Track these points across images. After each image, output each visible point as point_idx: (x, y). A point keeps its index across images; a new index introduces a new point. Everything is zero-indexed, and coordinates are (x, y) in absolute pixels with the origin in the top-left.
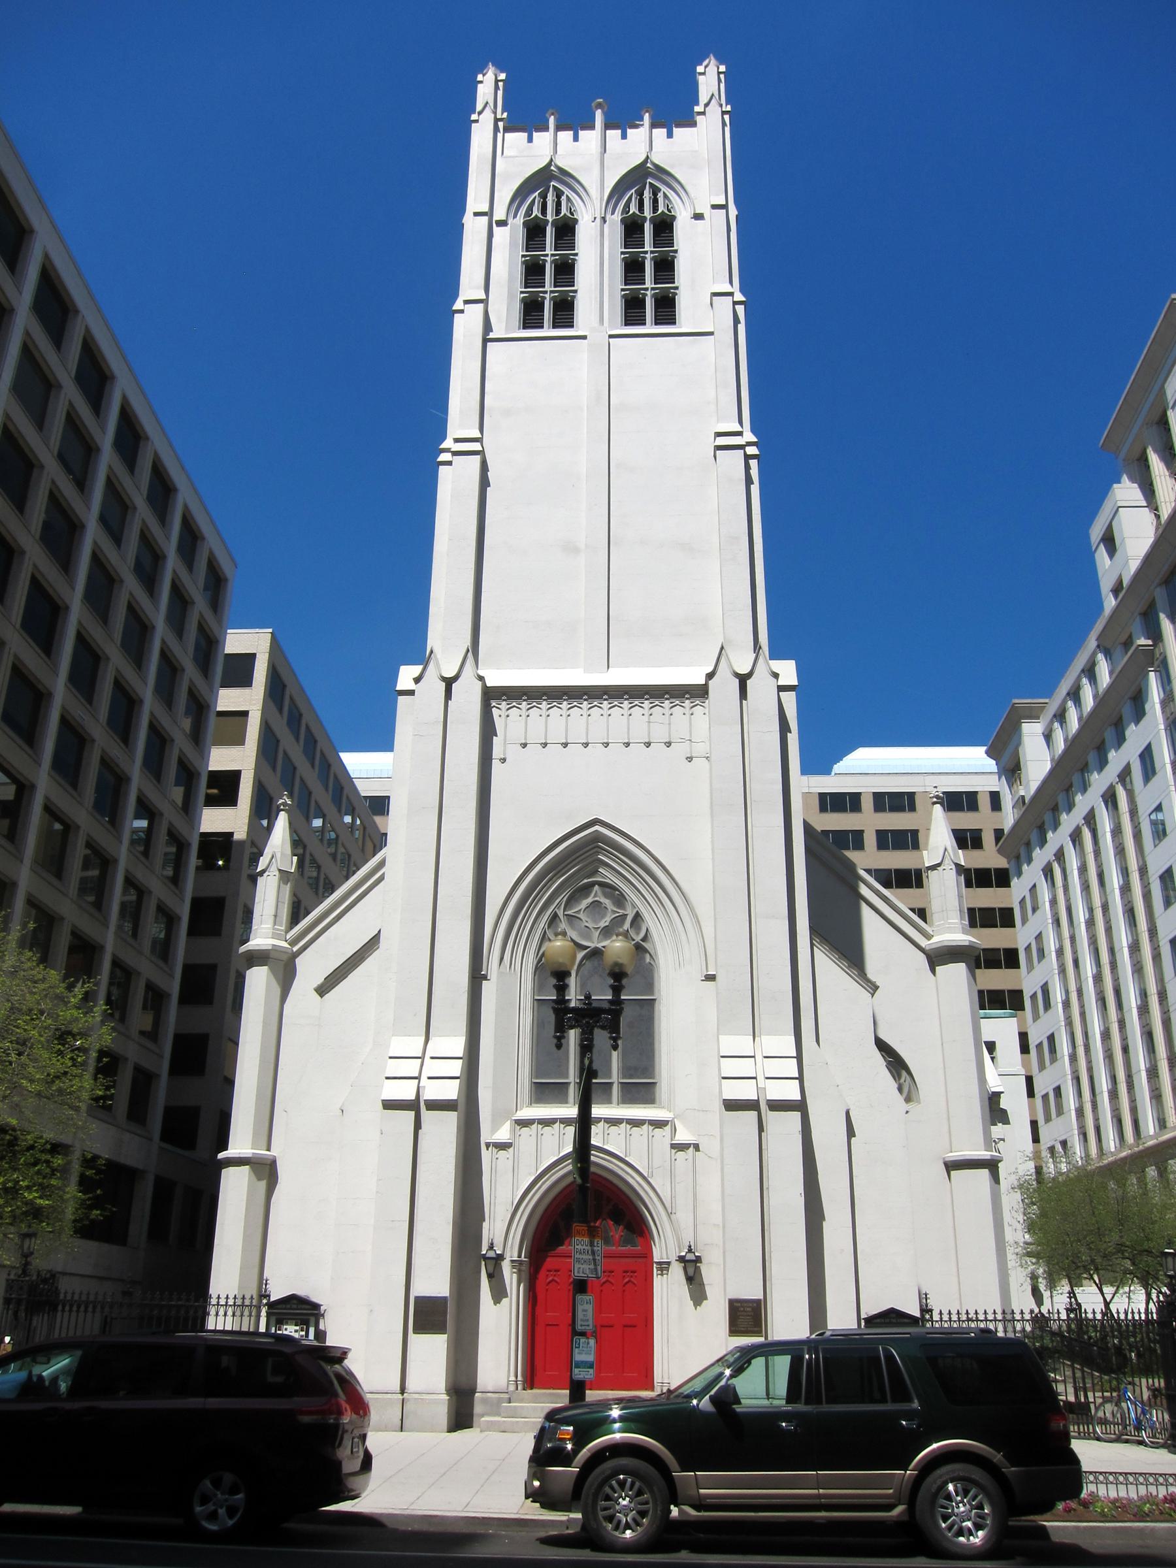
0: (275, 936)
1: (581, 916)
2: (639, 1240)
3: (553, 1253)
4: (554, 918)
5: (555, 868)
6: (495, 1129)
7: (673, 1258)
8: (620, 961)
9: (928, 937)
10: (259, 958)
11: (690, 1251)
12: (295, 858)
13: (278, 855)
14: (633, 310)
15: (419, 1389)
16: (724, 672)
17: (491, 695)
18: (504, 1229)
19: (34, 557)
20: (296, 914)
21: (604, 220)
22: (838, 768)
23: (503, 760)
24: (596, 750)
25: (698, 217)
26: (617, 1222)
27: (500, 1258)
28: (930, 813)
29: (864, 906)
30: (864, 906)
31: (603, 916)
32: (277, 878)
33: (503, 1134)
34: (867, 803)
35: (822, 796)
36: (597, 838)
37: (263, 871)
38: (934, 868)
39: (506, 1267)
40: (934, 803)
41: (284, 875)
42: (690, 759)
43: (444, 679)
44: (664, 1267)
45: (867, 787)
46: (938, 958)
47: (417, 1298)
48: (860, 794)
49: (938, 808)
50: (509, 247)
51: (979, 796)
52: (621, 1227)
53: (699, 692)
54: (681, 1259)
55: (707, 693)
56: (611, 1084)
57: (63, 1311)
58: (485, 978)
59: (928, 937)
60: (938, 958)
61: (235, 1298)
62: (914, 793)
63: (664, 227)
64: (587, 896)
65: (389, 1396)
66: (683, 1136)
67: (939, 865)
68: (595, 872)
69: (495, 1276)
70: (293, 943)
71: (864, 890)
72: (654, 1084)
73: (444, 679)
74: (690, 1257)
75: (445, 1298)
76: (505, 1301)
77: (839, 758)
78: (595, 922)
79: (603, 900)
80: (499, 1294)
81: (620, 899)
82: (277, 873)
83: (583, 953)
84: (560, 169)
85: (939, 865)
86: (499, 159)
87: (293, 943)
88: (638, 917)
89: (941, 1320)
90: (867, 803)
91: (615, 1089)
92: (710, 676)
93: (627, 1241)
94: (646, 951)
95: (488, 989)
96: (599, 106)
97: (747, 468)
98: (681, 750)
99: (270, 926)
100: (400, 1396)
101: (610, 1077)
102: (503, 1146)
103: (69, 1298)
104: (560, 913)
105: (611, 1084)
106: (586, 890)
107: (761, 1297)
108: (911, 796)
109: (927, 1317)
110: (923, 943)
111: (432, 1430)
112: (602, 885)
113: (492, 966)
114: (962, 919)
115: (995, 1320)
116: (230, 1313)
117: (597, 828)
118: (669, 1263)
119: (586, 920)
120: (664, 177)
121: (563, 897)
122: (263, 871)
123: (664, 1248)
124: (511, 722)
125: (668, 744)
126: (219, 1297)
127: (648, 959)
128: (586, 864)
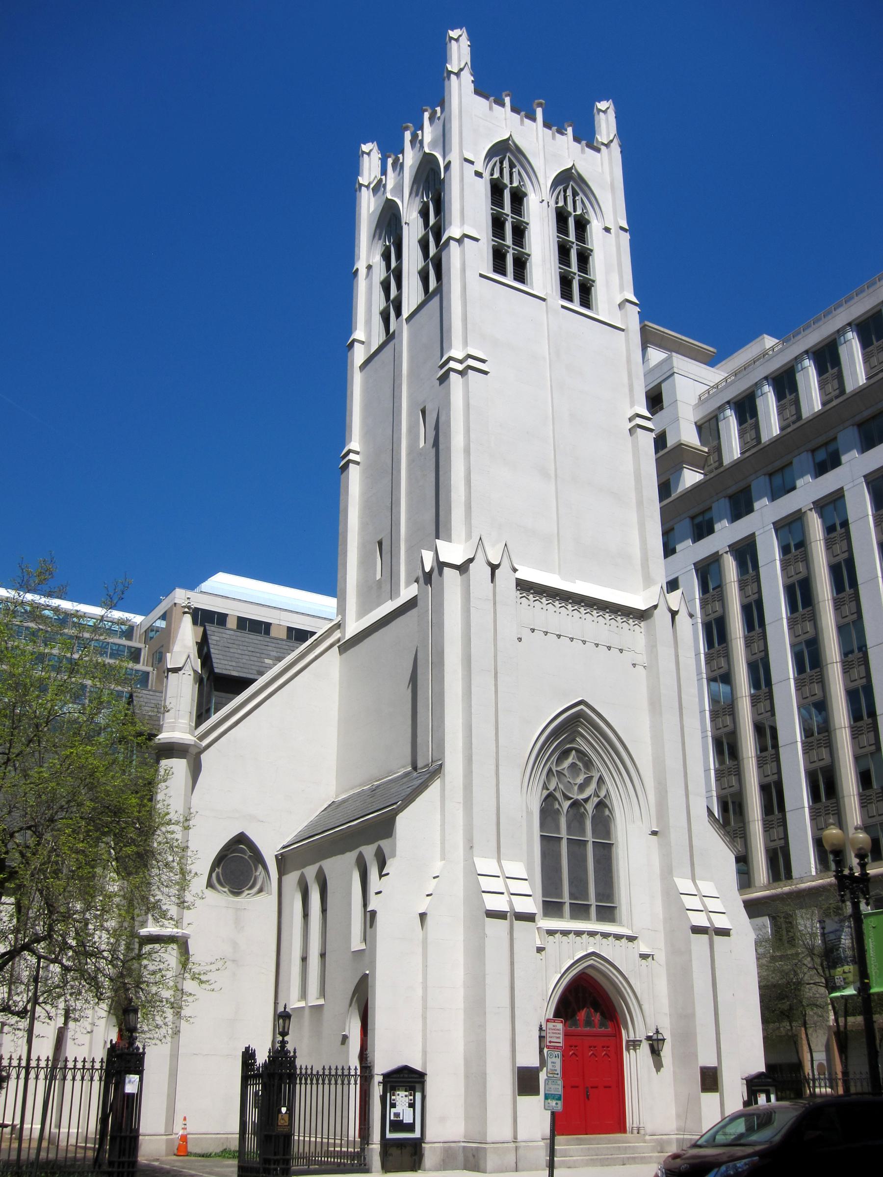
1: (566, 772)
2: (609, 1023)
4: (550, 770)
5: (555, 734)
7: (643, 1038)
10: (172, 750)
11: (657, 1032)
15: (493, 1140)
20: (202, 715)
22: (206, 586)
25: (607, 230)
28: (181, 620)
31: (578, 776)
38: (176, 670)
40: (185, 613)
42: (634, 665)
44: (634, 1044)
45: (234, 611)
49: (188, 619)
52: (598, 1014)
53: (642, 615)
54: (649, 1038)
56: (589, 906)
57: (301, 1084)
61: (84, 1061)
62: (270, 624)
65: (506, 1145)
66: (645, 950)
67: (180, 669)
68: (573, 740)
70: (202, 738)
72: (614, 908)
77: (205, 579)
79: (578, 763)
81: (588, 764)
82: (192, 673)
83: (569, 802)
85: (180, 669)
87: (202, 738)
88: (601, 780)
89: (10, 1066)
91: (593, 910)
93: (602, 1025)
94: (606, 806)
96: (540, 105)
100: (513, 1145)
101: (562, 898)
103: (309, 1072)
104: (554, 769)
105: (589, 906)
106: (565, 754)
108: (268, 625)
111: (537, 1169)
112: (578, 751)
114: (191, 720)
116: (78, 1077)
117: (582, 707)
118: (641, 1041)
120: (586, 189)
121: (555, 757)
123: (638, 1028)
125: (621, 651)
126: (75, 1061)
127: (607, 812)
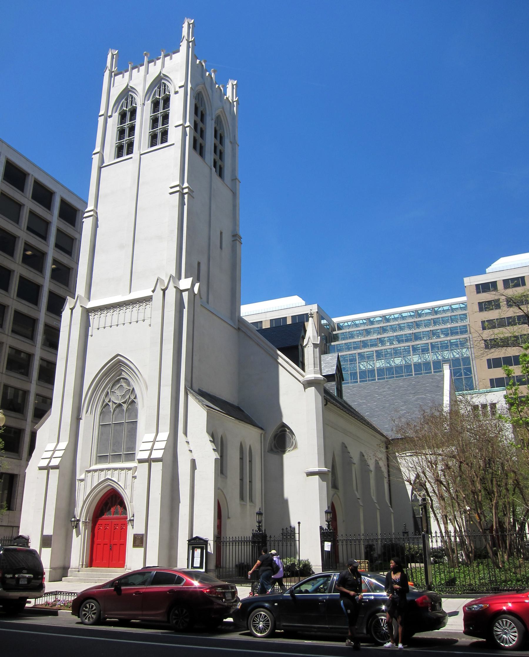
0: (315, 373)
3: (101, 518)
5: (106, 374)
6: (81, 475)
9: (303, 376)
12: (319, 337)
13: (311, 338)
17: (87, 312)
18: (82, 510)
21: (144, 104)
22: (488, 270)
23: (92, 336)
26: (121, 506)
27: (79, 520)
29: (280, 367)
30: (280, 366)
32: (312, 347)
33: (83, 477)
34: (500, 286)
35: (477, 286)
36: (120, 361)
37: (306, 345)
39: (81, 523)
41: (315, 346)
43: (162, 290)
45: (499, 278)
46: (308, 384)
48: (496, 281)
50: (113, 123)
51: (525, 278)
55: (152, 299)
58: (81, 419)
59: (303, 376)
60: (308, 384)
64: (119, 383)
69: (77, 526)
71: (280, 360)
73: (162, 290)
76: (80, 536)
80: (78, 534)
81: (129, 384)
84: (131, 87)
86: (114, 86)
88: (133, 389)
92: (153, 291)
95: (82, 422)
97: (183, 198)
98: (147, 322)
99: (313, 369)
102: (82, 480)
106: (118, 381)
107: (144, 533)
108: (523, 278)
113: (84, 415)
117: (119, 357)
121: (110, 385)
122: (306, 345)
124: (95, 320)
128: (116, 371)
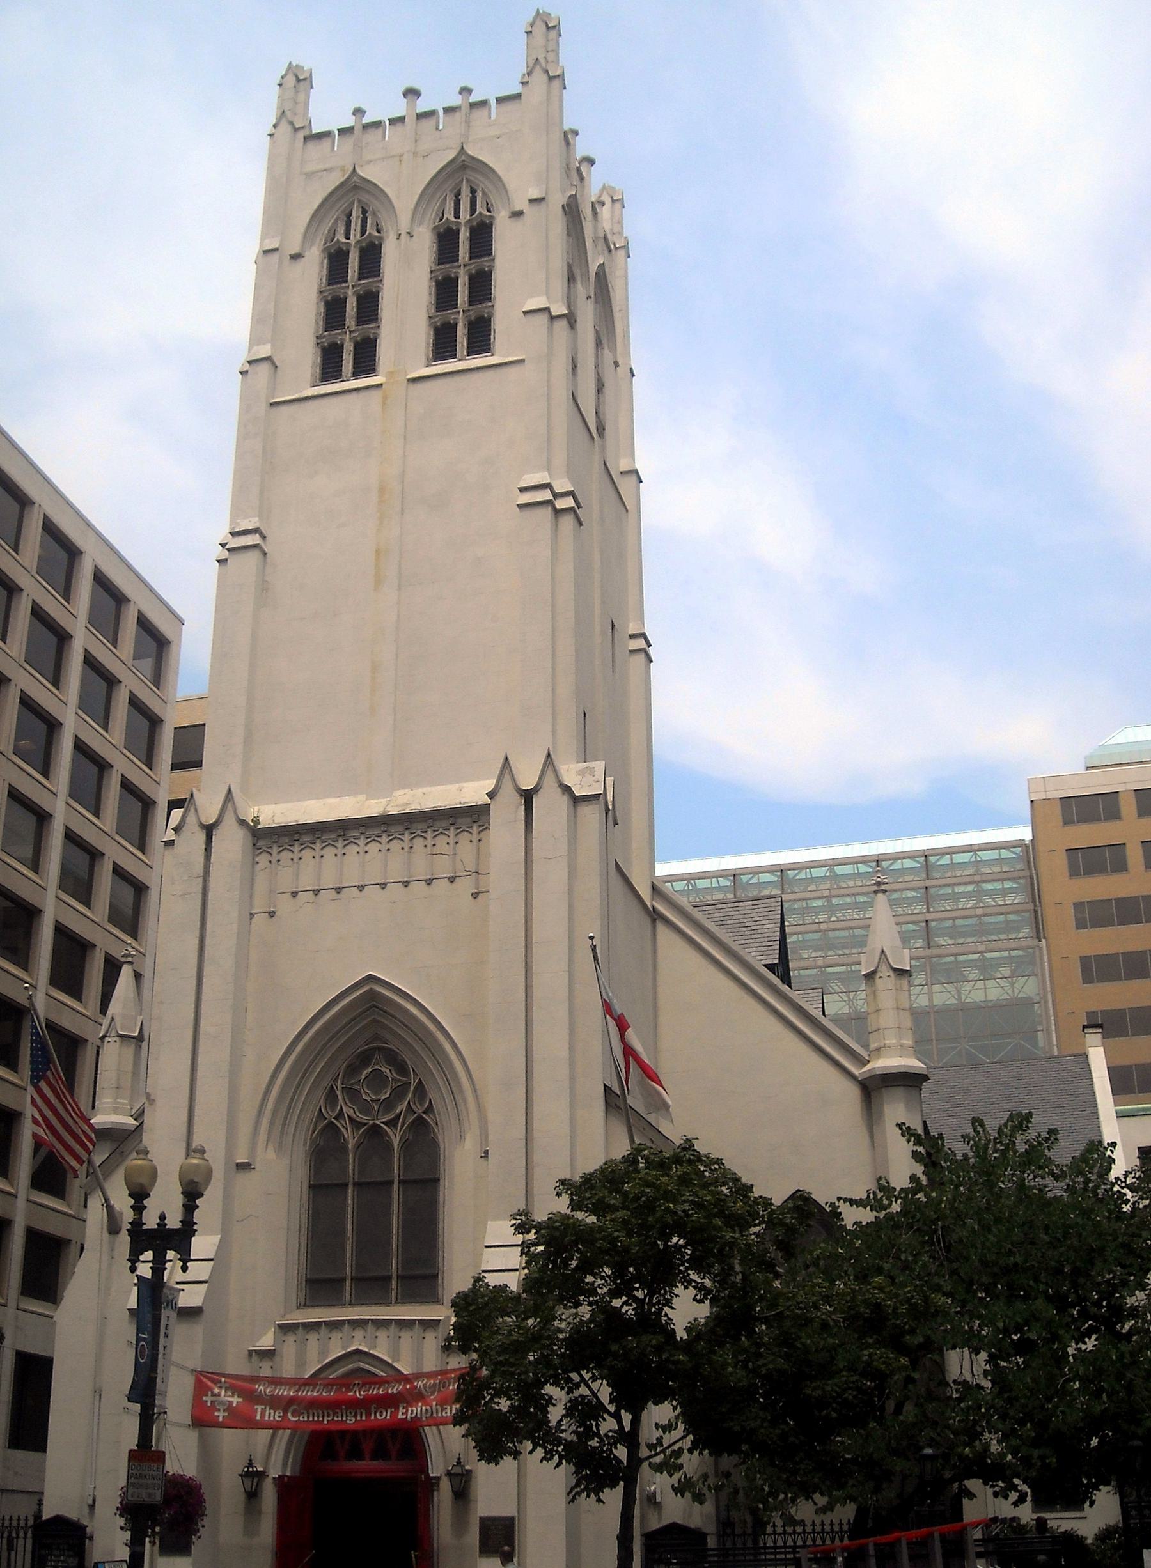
8: (196, 1180)
11: (459, 1462)
14: (443, 344)
16: (508, 790)
19: (34, 589)
24: (395, 890)
25: (518, 214)
31: (385, 1087)
34: (1128, 807)
47: (483, 1520)
54: (449, 1474)
63: (482, 236)
74: (458, 1470)
75: (962, 1520)
78: (375, 1093)
90: (1128, 807)
92: (491, 795)
109: (729, 1531)
110: (856, 1072)
115: (744, 1534)
119: (367, 1095)
